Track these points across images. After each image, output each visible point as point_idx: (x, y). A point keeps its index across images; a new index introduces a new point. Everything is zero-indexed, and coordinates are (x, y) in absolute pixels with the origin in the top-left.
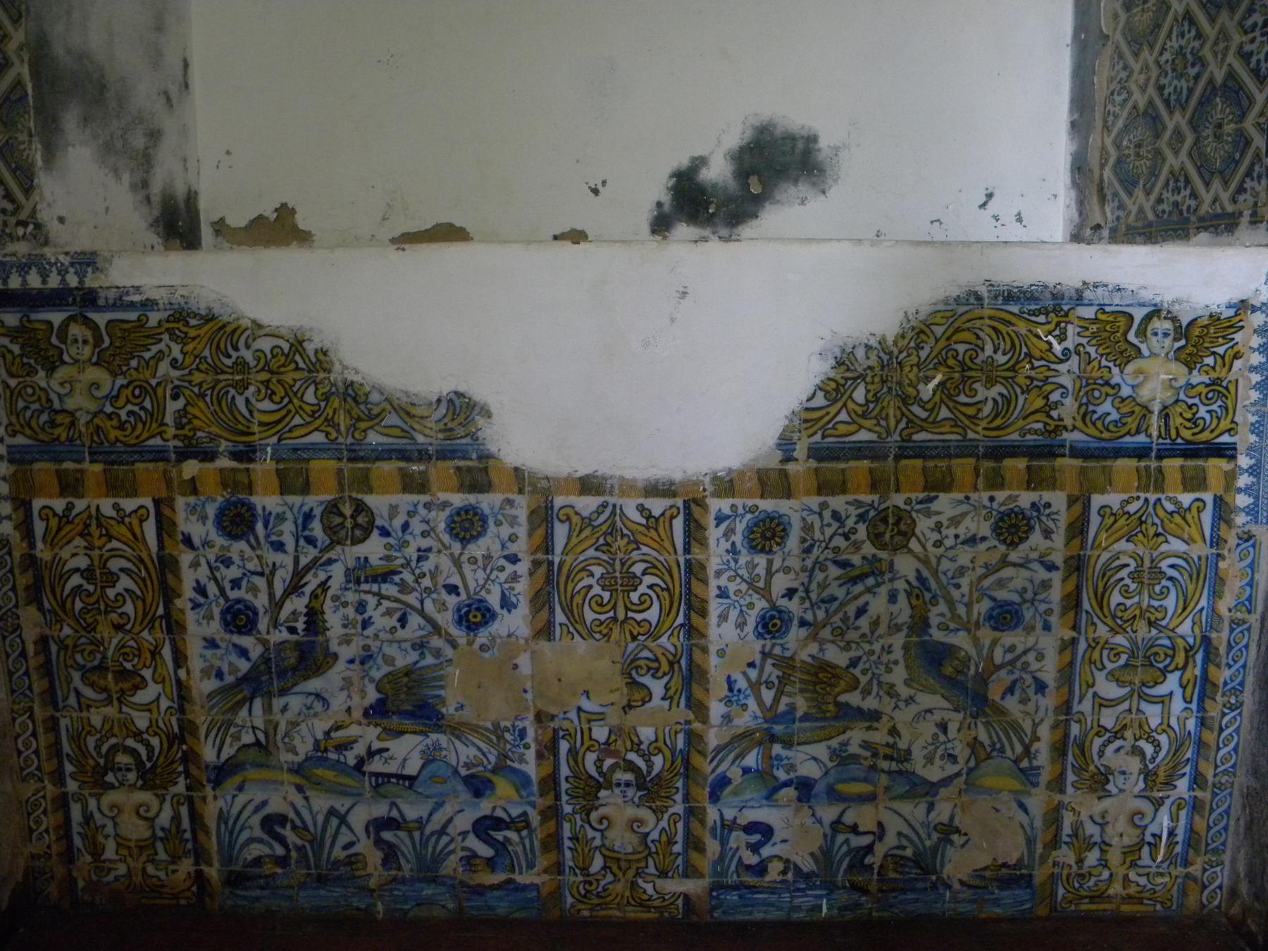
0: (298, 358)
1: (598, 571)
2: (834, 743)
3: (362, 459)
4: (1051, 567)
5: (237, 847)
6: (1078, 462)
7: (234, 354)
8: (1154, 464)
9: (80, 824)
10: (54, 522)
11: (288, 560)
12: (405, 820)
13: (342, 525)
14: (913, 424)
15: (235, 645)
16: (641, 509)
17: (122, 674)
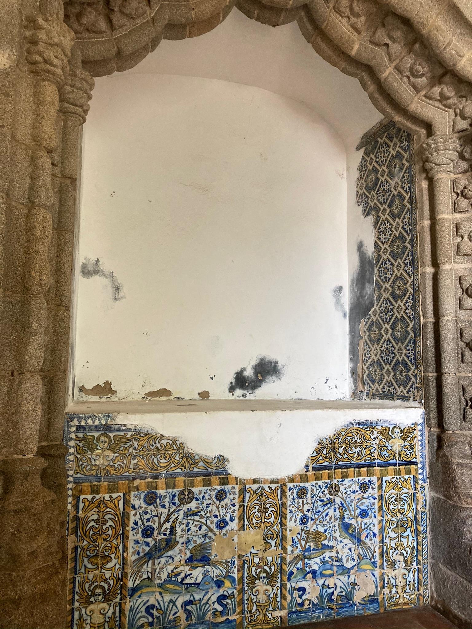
0: (174, 446)
1: (257, 507)
2: (321, 557)
3: (192, 477)
4: (375, 498)
5: (137, 618)
6: (379, 468)
7: (155, 445)
8: (398, 468)
9: (77, 620)
10: (87, 504)
11: (166, 511)
12: (195, 601)
13: (184, 498)
14: (338, 460)
15: (145, 542)
16: (269, 487)
17: (104, 557)
